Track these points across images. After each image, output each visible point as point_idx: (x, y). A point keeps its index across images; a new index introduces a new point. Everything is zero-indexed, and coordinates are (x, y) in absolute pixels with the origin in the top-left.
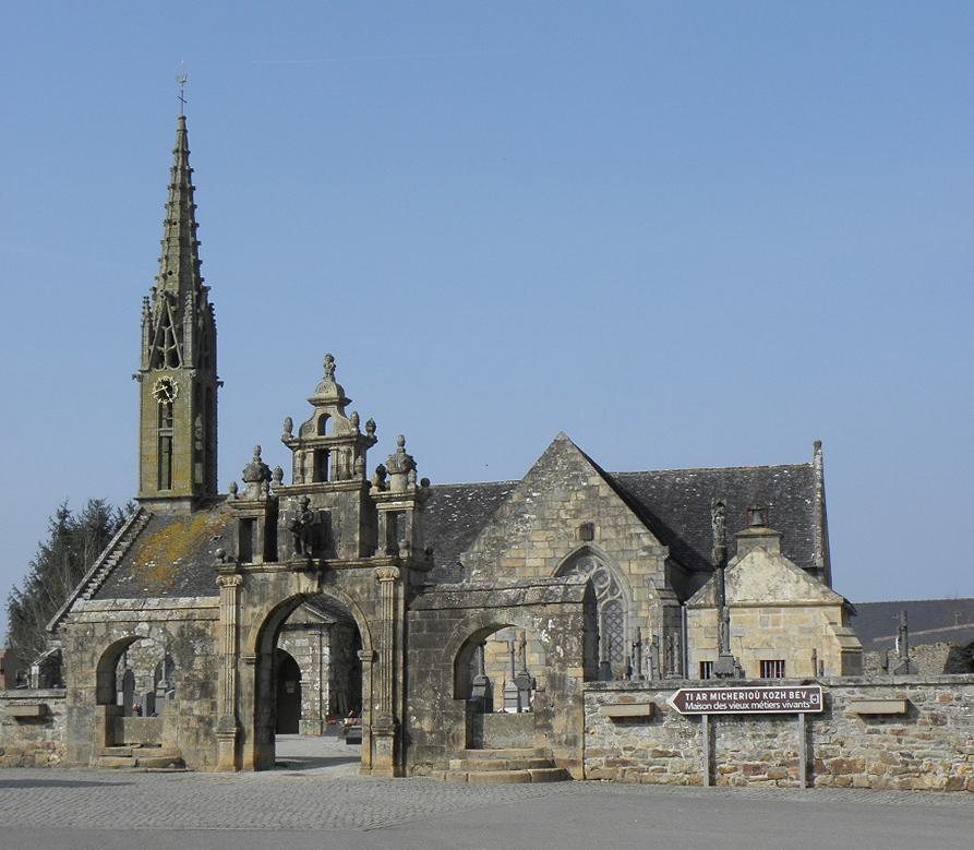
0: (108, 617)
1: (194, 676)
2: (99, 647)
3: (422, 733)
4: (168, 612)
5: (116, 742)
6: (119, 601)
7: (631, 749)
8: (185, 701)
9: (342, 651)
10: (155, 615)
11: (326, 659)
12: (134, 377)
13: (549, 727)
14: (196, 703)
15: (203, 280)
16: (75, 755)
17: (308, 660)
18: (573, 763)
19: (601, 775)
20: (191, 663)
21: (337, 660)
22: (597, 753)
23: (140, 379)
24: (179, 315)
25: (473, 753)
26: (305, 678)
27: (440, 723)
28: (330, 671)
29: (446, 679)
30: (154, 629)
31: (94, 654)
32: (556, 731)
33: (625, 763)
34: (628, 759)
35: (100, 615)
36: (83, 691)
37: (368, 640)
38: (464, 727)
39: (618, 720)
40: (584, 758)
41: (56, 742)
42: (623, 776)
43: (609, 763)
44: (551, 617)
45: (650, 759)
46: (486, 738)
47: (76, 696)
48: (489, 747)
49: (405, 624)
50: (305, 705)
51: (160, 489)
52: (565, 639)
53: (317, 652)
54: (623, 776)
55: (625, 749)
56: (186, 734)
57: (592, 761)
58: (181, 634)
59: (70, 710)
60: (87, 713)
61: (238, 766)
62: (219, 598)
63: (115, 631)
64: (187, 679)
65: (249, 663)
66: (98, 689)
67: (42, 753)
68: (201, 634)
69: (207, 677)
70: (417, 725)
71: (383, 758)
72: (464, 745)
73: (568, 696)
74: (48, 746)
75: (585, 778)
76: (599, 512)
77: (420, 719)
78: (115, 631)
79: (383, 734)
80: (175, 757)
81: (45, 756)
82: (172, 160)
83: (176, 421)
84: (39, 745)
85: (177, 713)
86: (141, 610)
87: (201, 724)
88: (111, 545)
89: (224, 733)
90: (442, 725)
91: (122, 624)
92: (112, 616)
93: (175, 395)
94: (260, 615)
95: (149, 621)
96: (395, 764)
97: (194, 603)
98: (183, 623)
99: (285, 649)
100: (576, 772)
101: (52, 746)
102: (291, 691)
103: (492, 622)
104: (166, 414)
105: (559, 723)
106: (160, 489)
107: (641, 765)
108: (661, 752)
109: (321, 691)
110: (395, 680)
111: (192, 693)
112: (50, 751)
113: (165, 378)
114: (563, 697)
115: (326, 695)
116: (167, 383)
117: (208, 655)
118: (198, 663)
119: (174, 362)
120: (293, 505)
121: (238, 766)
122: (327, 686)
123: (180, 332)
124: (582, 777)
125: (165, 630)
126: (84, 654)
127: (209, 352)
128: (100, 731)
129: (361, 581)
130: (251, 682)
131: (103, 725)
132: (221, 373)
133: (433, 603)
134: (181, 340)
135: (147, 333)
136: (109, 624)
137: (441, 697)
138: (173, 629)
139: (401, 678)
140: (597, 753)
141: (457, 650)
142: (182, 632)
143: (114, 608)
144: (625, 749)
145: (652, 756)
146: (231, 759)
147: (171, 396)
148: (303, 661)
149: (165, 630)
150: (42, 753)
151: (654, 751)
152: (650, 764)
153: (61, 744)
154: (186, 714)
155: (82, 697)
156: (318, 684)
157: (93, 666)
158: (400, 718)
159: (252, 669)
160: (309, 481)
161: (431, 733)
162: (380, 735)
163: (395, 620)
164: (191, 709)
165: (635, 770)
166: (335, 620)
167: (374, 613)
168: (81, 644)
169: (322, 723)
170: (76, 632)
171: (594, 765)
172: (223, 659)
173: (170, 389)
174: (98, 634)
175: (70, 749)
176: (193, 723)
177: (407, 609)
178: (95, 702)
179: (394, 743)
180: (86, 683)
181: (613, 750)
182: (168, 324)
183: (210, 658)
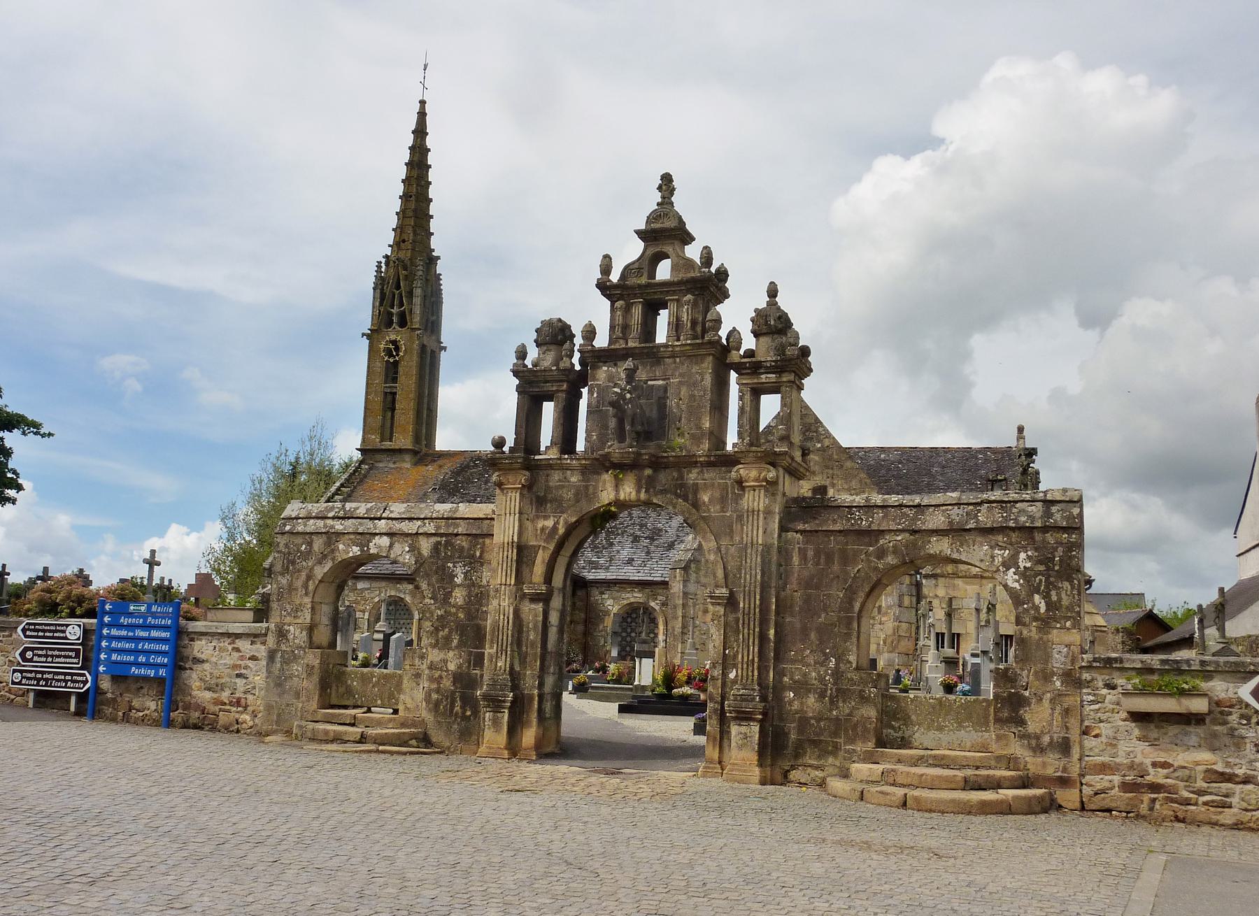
0: (332, 527)
4: (419, 523)
6: (348, 506)
7: (1165, 765)
8: (436, 651)
10: (398, 526)
12: (363, 335)
13: (1022, 722)
14: (451, 654)
15: (433, 250)
18: (1064, 782)
19: (1113, 805)
20: (448, 595)
22: (1103, 768)
23: (368, 336)
24: (410, 278)
30: (397, 545)
32: (1032, 727)
33: (1155, 788)
34: (1162, 781)
35: (320, 523)
39: (1139, 717)
40: (1082, 775)
41: (250, 697)
42: (1151, 809)
43: (1126, 787)
45: (1201, 784)
47: (282, 634)
51: (382, 441)
52: (1048, 583)
54: (1151, 809)
55: (1154, 765)
57: (1097, 781)
59: (271, 656)
60: (296, 658)
61: (513, 750)
62: (492, 506)
63: (341, 547)
64: (440, 618)
67: (229, 711)
73: (1053, 674)
74: (238, 703)
75: (1083, 808)
76: (833, 474)
79: (744, 717)
82: (410, 140)
83: (402, 378)
85: (424, 667)
86: (380, 519)
88: (333, 489)
89: (495, 703)
91: (352, 537)
92: (339, 526)
93: (401, 354)
95: (390, 535)
97: (456, 510)
100: (1068, 797)
101: (243, 701)
104: (392, 371)
105: (1039, 717)
106: (382, 441)
107: (1186, 794)
108: (1222, 774)
110: (763, 638)
111: (448, 639)
112: (240, 709)
113: (393, 337)
114: (1046, 677)
116: (394, 342)
118: (459, 596)
119: (403, 323)
120: (611, 378)
123: (410, 294)
124: (1078, 805)
127: (434, 318)
128: (310, 685)
129: (713, 485)
132: (445, 338)
134: (411, 303)
135: (378, 295)
136: (332, 537)
137: (837, 664)
138: (426, 546)
140: (1103, 768)
143: (341, 514)
144: (1154, 765)
145: (1204, 780)
146: (502, 738)
147: (398, 355)
150: (229, 711)
151: (1207, 771)
152: (1201, 793)
153: (256, 701)
154: (436, 669)
162: (735, 719)
164: (445, 661)
165: (1173, 801)
168: (293, 563)
171: (1099, 787)
173: (397, 349)
175: (269, 708)
179: (761, 732)
181: (1131, 767)
182: (398, 287)
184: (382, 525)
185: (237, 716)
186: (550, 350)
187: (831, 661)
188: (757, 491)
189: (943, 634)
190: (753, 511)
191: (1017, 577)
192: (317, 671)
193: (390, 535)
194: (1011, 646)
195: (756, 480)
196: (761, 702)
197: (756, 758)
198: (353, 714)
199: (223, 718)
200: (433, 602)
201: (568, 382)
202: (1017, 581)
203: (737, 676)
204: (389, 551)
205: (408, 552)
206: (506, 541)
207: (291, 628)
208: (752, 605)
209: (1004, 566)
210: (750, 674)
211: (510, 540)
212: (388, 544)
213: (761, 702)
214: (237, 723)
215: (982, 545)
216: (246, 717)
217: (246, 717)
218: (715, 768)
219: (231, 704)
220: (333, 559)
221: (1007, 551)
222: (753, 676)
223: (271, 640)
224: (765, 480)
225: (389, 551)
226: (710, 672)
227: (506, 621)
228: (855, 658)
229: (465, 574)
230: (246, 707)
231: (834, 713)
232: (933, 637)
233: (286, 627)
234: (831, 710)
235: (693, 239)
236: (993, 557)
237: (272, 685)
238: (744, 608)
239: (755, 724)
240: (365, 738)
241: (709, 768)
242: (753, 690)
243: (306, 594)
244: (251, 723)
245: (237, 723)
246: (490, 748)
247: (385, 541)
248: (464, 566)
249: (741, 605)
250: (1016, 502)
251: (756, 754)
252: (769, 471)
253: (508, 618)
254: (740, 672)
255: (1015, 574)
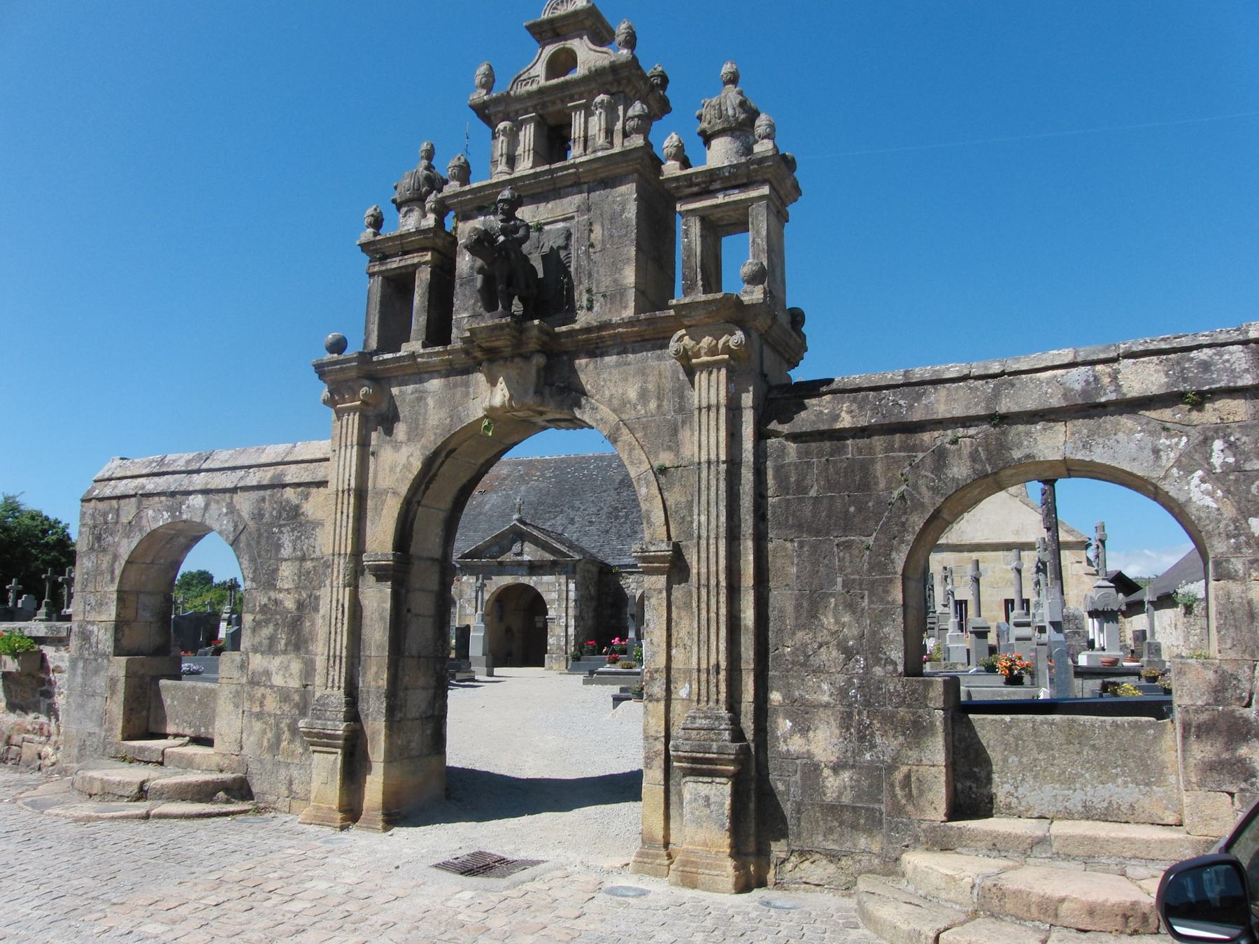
1: (276, 602)
2: (125, 542)
3: (812, 770)
5: (153, 728)
8: (258, 656)
9: (588, 588)
11: (572, 595)
16: (75, 752)
17: (554, 595)
21: (582, 596)
25: (975, 836)
26: (552, 613)
27: (864, 738)
28: (576, 607)
29: (882, 617)
30: (213, 506)
31: (115, 557)
36: (95, 628)
37: (658, 516)
38: (940, 758)
44: (1221, 430)
46: (1001, 790)
47: (85, 636)
48: (1010, 812)
49: (759, 473)
50: (551, 641)
53: (564, 588)
56: (258, 726)
58: (258, 516)
59: (74, 663)
61: (351, 813)
64: (264, 609)
65: (381, 574)
66: (120, 625)
68: (293, 514)
69: (300, 605)
70: (796, 744)
71: (701, 835)
72: (942, 808)
77: (803, 728)
78: (150, 512)
79: (701, 768)
80: (227, 776)
81: (36, 748)
84: (29, 727)
85: (244, 680)
87: (286, 708)
90: (873, 746)
94: (407, 467)
96: (737, 852)
98: (262, 493)
99: (532, 585)
102: (540, 625)
103: (1017, 454)
109: (567, 626)
112: (43, 739)
115: (571, 631)
117: (303, 559)
121: (351, 813)
122: (572, 622)
125: (232, 509)
126: (101, 555)
130: (382, 618)
131: (120, 696)
133: (836, 418)
138: (245, 503)
139: (748, 616)
141: (910, 538)
142: (260, 510)
148: (550, 596)
149: (232, 509)
155: (94, 640)
156: (564, 620)
157: (112, 580)
158: (748, 724)
159: (387, 589)
160: (525, 166)
161: (837, 768)
163: (734, 463)
166: (581, 557)
167: (674, 446)
169: (567, 660)
170: (93, 515)
172: (328, 565)
174: (124, 519)
176: (271, 705)
177: (761, 435)
178: (111, 650)
180: (100, 613)
183: (309, 564)
184: (199, 481)
185: (40, 747)
186: (411, 210)
187: (857, 661)
188: (715, 371)
189: (1012, 601)
190: (709, 408)
191: (1208, 486)
192: (121, 686)
193: (205, 492)
194: (1013, 610)
195: (712, 351)
196: (733, 741)
197: (728, 841)
198: (161, 748)
199: (28, 752)
200: (254, 586)
201: (433, 249)
202: (1211, 494)
203: (690, 694)
204: (204, 515)
205: (227, 514)
206: (340, 489)
207: (95, 628)
208: (713, 569)
209: (1180, 468)
210: (713, 689)
211: (346, 487)
212: (203, 505)
213: (733, 741)
214: (40, 758)
215: (1131, 432)
216: (48, 750)
217: (48, 750)
218: (658, 856)
219: (34, 732)
220: (140, 530)
221: (1184, 439)
222: (718, 693)
223: (74, 642)
224: (727, 349)
225: (204, 515)
226: (645, 689)
227: (340, 611)
228: (901, 654)
229: (294, 542)
230: (49, 736)
231: (868, 756)
232: (952, 604)
233: (90, 627)
234: (861, 753)
235: (640, 800)
236: (1156, 451)
237: (74, 706)
238: (699, 574)
239: (723, 780)
240: (147, 792)
241: (647, 855)
242: (718, 718)
243: (112, 580)
244: (53, 759)
245: (40, 758)
246: (319, 808)
247: (198, 501)
248: (293, 530)
249: (694, 571)
250: (1190, 349)
251: (728, 833)
252: (732, 334)
253: (343, 606)
254: (695, 686)
255: (1203, 481)
